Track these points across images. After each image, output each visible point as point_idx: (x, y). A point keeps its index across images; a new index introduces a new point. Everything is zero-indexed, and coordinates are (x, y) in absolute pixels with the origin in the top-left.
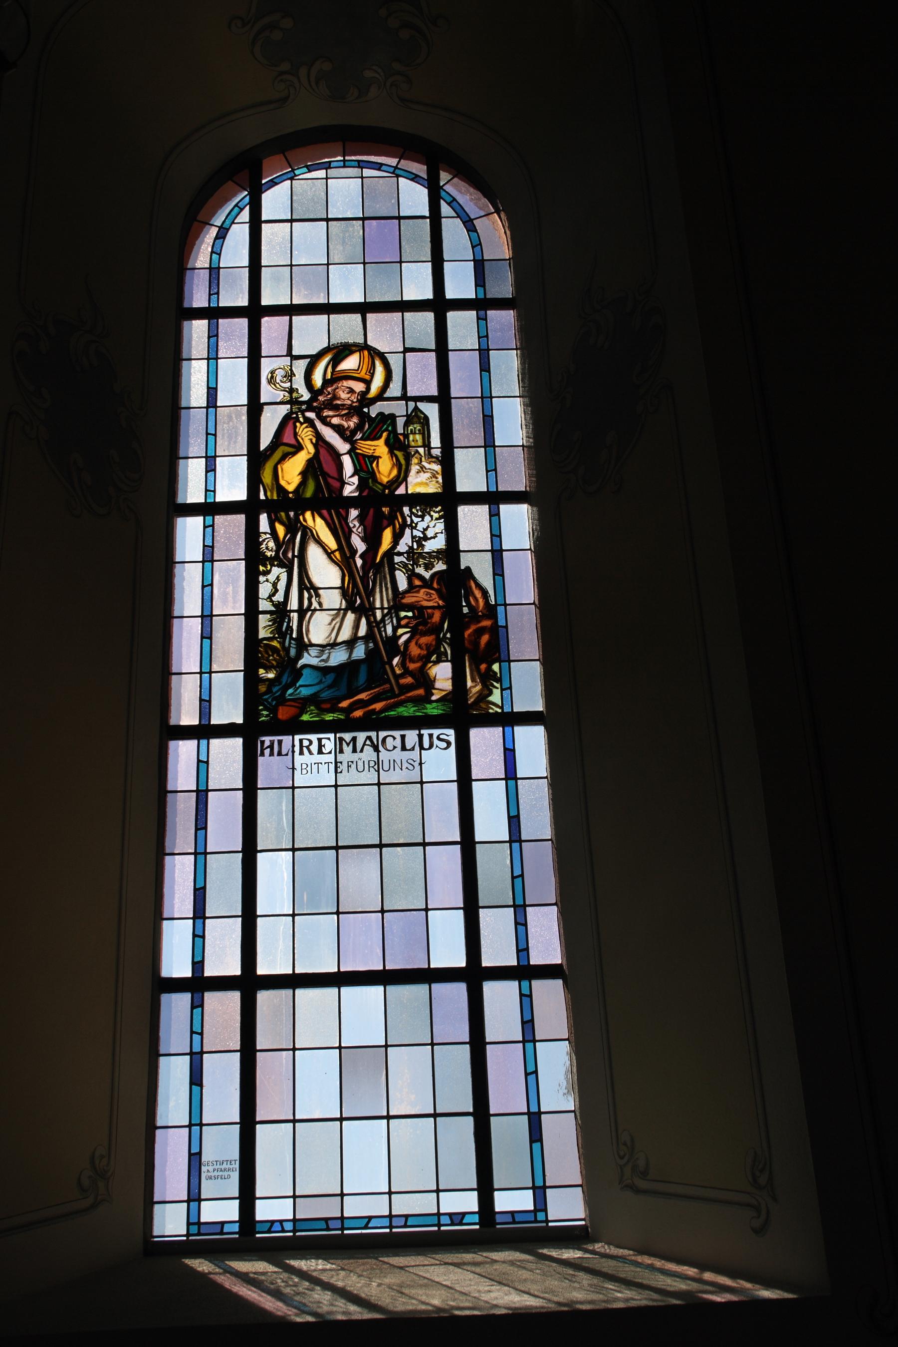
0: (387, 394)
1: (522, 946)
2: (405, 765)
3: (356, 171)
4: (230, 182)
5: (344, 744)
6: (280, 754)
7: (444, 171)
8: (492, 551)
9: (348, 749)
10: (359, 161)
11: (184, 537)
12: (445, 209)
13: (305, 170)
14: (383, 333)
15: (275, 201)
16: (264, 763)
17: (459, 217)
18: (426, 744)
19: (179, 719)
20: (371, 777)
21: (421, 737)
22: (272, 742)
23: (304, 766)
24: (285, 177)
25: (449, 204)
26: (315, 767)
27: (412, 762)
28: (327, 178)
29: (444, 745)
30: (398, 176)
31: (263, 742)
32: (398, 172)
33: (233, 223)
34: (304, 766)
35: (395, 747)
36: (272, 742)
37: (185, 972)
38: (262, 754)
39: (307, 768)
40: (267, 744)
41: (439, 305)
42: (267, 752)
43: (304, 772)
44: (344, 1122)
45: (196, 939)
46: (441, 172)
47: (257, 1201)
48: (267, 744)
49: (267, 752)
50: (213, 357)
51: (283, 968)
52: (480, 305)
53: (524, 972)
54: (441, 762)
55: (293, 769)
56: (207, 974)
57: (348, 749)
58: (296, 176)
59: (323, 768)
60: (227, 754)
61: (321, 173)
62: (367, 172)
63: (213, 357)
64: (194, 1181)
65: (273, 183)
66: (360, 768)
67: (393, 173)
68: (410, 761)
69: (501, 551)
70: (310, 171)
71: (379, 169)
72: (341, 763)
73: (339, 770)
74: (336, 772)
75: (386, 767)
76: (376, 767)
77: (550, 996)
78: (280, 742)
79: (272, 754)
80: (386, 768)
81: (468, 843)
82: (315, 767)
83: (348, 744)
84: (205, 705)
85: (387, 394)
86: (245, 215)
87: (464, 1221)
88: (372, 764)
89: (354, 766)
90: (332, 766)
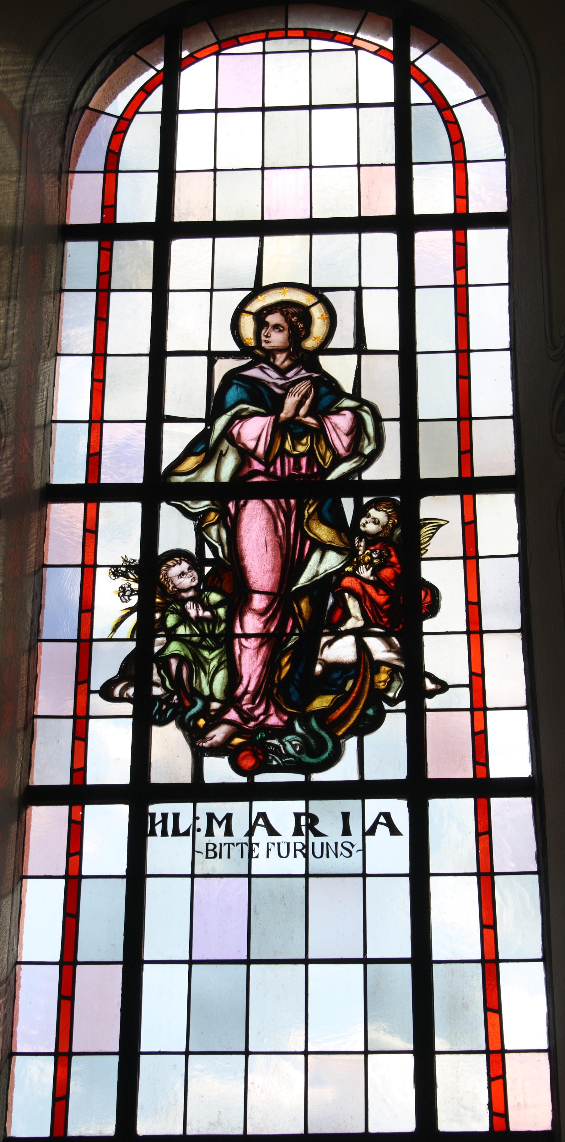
0: (332, 345)
1: (469, 518)
3: (303, 44)
5: (215, 823)
6: (176, 832)
7: (415, 47)
8: (455, 286)
9: (219, 831)
10: (305, 30)
11: (23, 925)
12: (417, 94)
14: (334, 259)
15: (196, 83)
16: (155, 846)
19: (27, 872)
22: (165, 816)
23: (211, 847)
24: (207, 51)
25: (422, 85)
26: (225, 849)
27: (350, 847)
28: (264, 53)
30: (356, 49)
31: (153, 815)
32: (356, 42)
33: (137, 112)
34: (211, 847)
36: (165, 816)
37: (77, 476)
38: (153, 834)
39: (214, 852)
40: (158, 818)
41: (405, 224)
42: (159, 829)
43: (211, 854)
44: (266, 113)
45: (476, 600)
46: (412, 48)
47: (142, 1057)
48: (158, 818)
49: (159, 829)
50: (103, 291)
51: (202, 214)
53: (482, 788)
56: (120, 220)
57: (219, 831)
59: (235, 851)
61: (258, 47)
62: (316, 44)
63: (103, 291)
64: (97, 401)
65: (193, 59)
66: (284, 853)
67: (350, 44)
68: (345, 845)
69: (503, 1051)
72: (258, 844)
73: (254, 855)
74: (250, 857)
76: (304, 851)
77: (514, 818)
78: (176, 816)
79: (164, 833)
80: (318, 853)
82: (225, 849)
83: (220, 824)
84: (94, 459)
85: (332, 345)
86: (155, 100)
87: (378, 48)
90: (246, 849)
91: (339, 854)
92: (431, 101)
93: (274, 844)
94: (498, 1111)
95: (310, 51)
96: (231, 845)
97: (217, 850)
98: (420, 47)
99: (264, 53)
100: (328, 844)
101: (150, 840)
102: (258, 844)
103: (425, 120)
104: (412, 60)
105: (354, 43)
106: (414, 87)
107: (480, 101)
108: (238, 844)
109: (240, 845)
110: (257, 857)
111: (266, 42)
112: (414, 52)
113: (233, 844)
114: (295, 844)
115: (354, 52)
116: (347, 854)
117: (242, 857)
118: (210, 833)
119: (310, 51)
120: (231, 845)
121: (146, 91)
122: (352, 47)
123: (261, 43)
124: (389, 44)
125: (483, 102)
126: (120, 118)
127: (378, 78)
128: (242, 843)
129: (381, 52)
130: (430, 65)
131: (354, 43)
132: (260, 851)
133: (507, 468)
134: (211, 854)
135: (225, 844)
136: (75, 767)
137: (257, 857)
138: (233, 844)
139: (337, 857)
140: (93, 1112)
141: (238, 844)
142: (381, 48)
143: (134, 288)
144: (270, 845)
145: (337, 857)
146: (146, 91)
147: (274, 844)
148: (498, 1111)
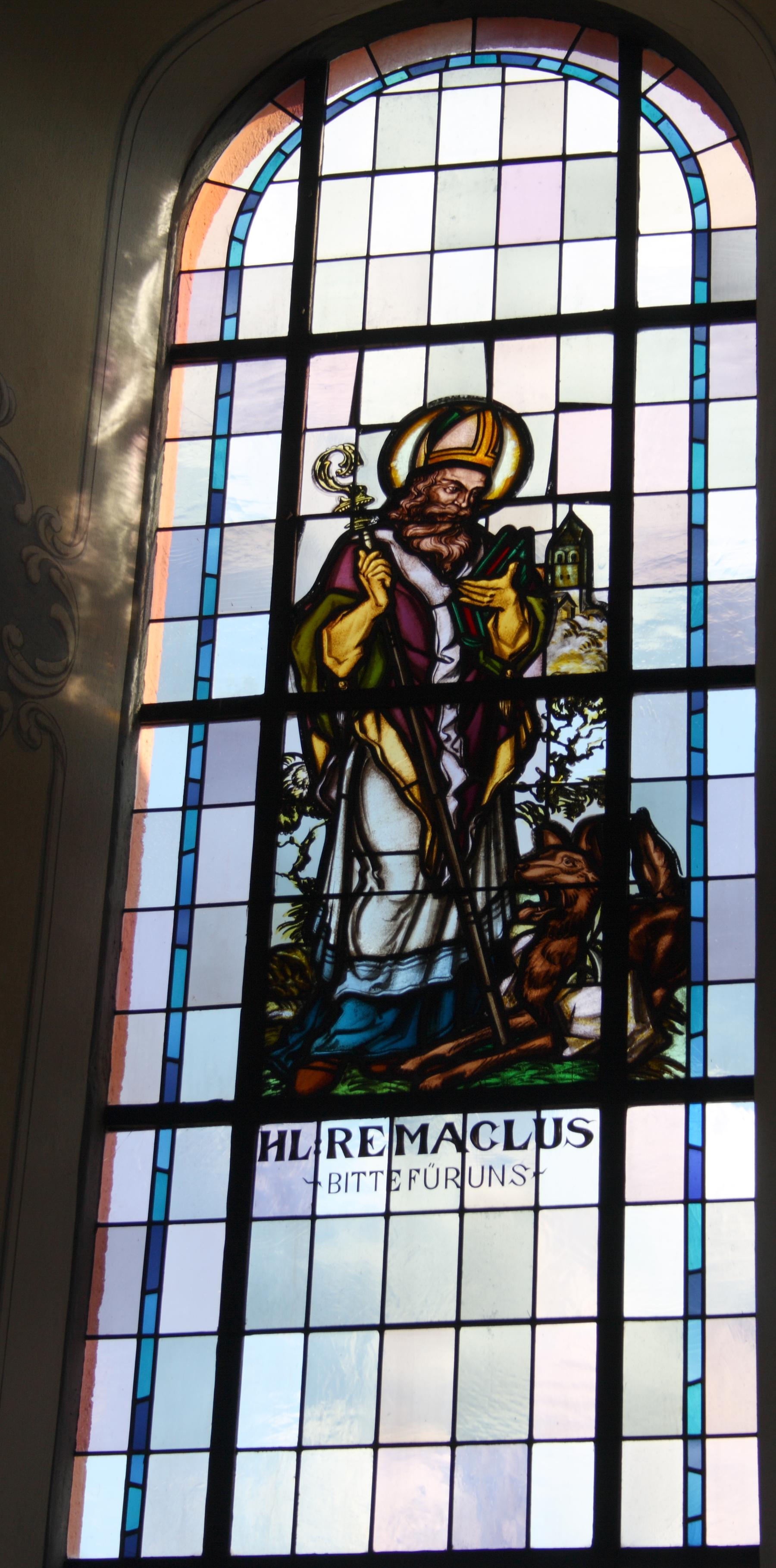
2: (509, 1175)
3: (495, 74)
4: (270, 105)
6: (294, 1156)
10: (498, 54)
12: (648, 136)
13: (403, 75)
15: (345, 140)
17: (671, 149)
18: (548, 1139)
20: (449, 1198)
21: (540, 1124)
22: (282, 1135)
23: (335, 1178)
25: (655, 126)
26: (353, 1180)
28: (440, 89)
29: (580, 1138)
30: (567, 78)
31: (266, 1135)
32: (568, 70)
33: (271, 182)
34: (335, 1178)
35: (493, 1144)
38: (264, 1157)
42: (273, 1152)
49: (273, 1152)
52: (699, 316)
54: (573, 1170)
55: (316, 1183)
58: (386, 87)
59: (367, 1181)
60: (206, 1152)
61: (432, 81)
62: (513, 74)
66: (431, 1182)
70: (411, 78)
71: (534, 67)
72: (398, 1172)
73: (394, 1186)
74: (389, 1189)
75: (476, 1181)
76: (458, 1180)
78: (296, 1135)
79: (280, 1157)
81: (610, 1321)
82: (353, 1180)
83: (412, 1139)
86: (292, 168)
88: (452, 1174)
89: (420, 1178)
90: (383, 1179)
91: (507, 1180)
92: (429, 400)
93: (418, 1171)
94: (694, 1518)
95: (503, 84)
96: (361, 1175)
97: (342, 1183)
98: (653, 75)
99: (440, 89)
100: (491, 1168)
101: (259, 1165)
102: (398, 1172)
103: (658, 174)
104: (643, 89)
105: (564, 71)
106: (645, 127)
107: (730, 145)
108: (371, 1173)
109: (374, 1174)
110: (397, 1189)
111: (445, 74)
112: (647, 80)
113: (364, 1173)
114: (330, 1175)
115: (563, 83)
116: (519, 1180)
117: (470, 1169)
118: (331, 1154)
119: (503, 84)
120: (361, 1175)
121: (267, 176)
122: (561, 77)
123: (437, 76)
124: (611, 68)
125: (735, 146)
126: (249, 192)
127: (595, 116)
128: (376, 1173)
129: (596, 80)
130: (664, 97)
131: (564, 71)
132: (401, 1180)
133: (745, 654)
134: (334, 1188)
135: (353, 1174)
136: (701, 715)
137: (397, 1189)
138: (364, 1173)
139: (503, 1183)
140: (173, 1527)
141: (371, 1173)
142: (601, 76)
143: (170, 533)
144: (414, 1173)
145: (503, 1183)
146: (282, 153)
147: (418, 1171)
148: (694, 1518)
